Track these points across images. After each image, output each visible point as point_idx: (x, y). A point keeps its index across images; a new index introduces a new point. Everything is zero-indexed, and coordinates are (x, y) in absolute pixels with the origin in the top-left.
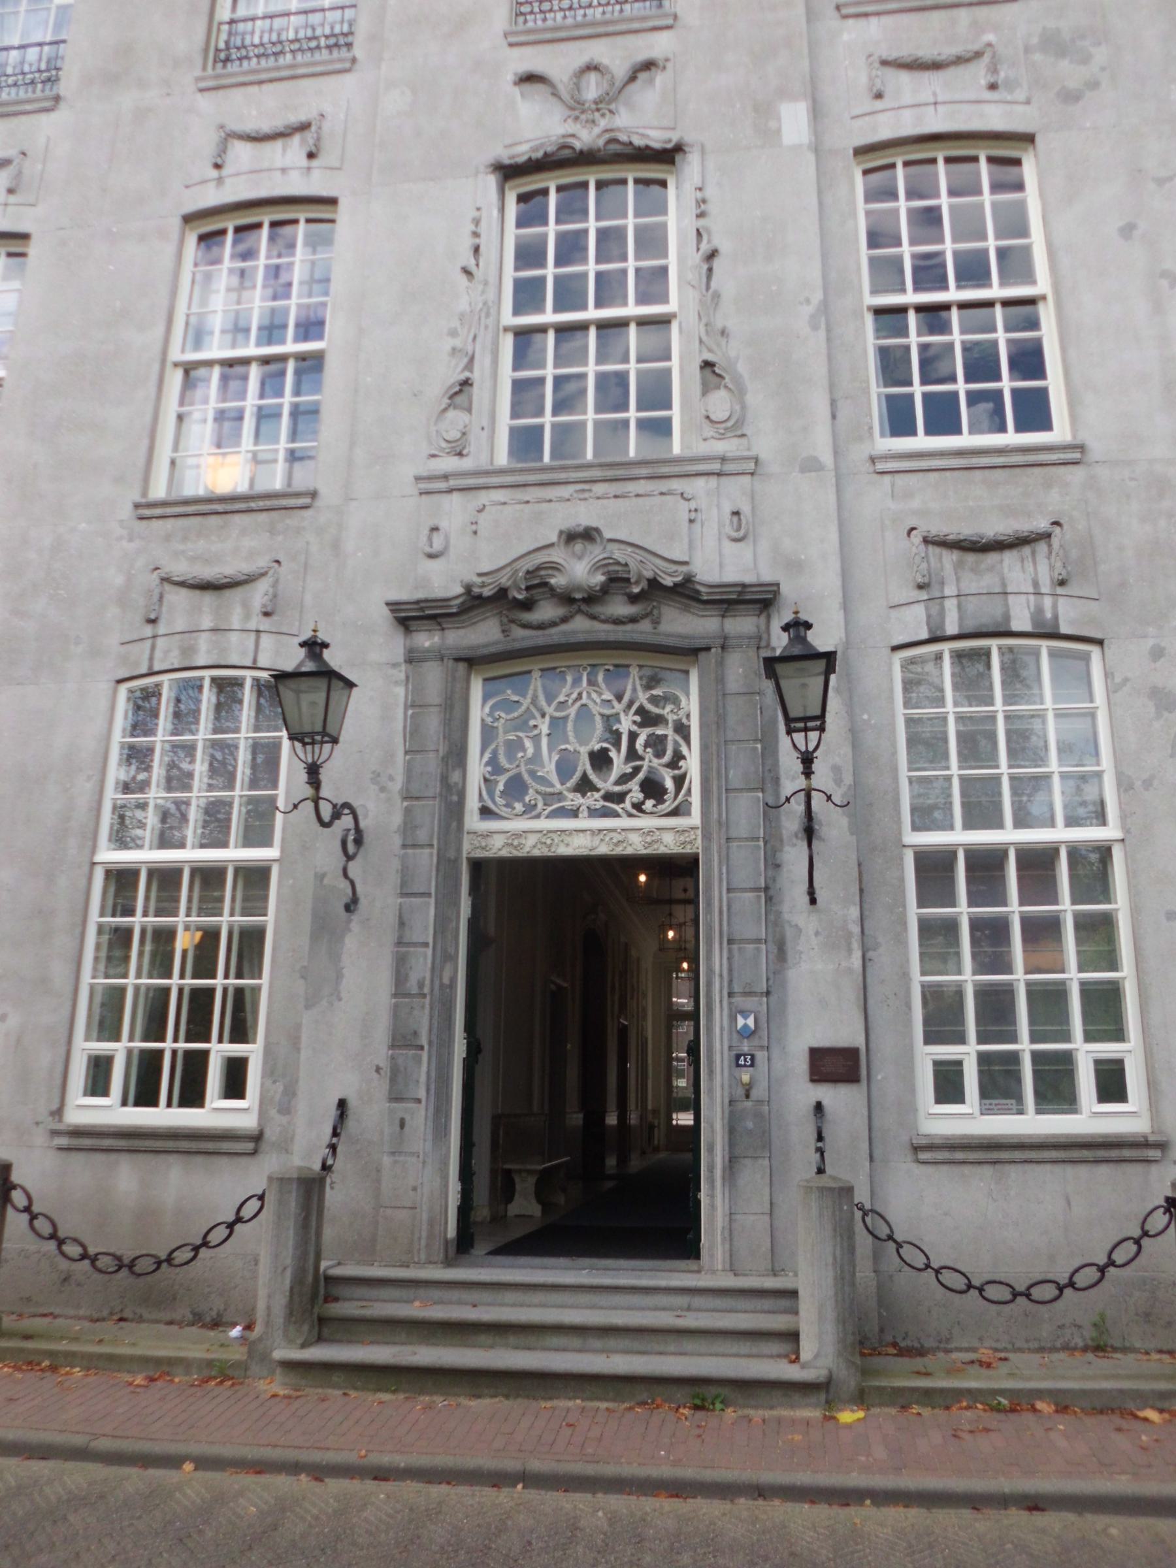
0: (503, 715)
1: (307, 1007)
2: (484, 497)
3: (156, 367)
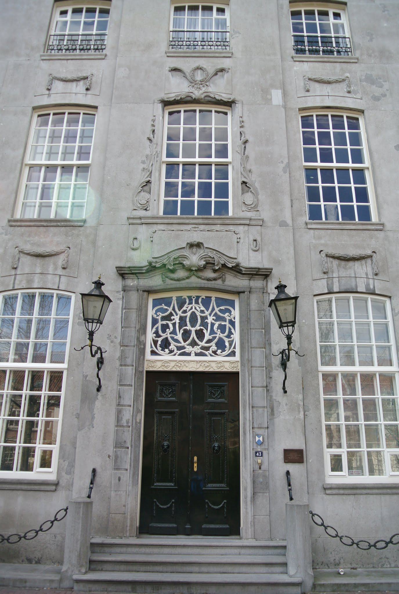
0: (161, 314)
1: (79, 430)
2: (155, 227)
3: (19, 165)
